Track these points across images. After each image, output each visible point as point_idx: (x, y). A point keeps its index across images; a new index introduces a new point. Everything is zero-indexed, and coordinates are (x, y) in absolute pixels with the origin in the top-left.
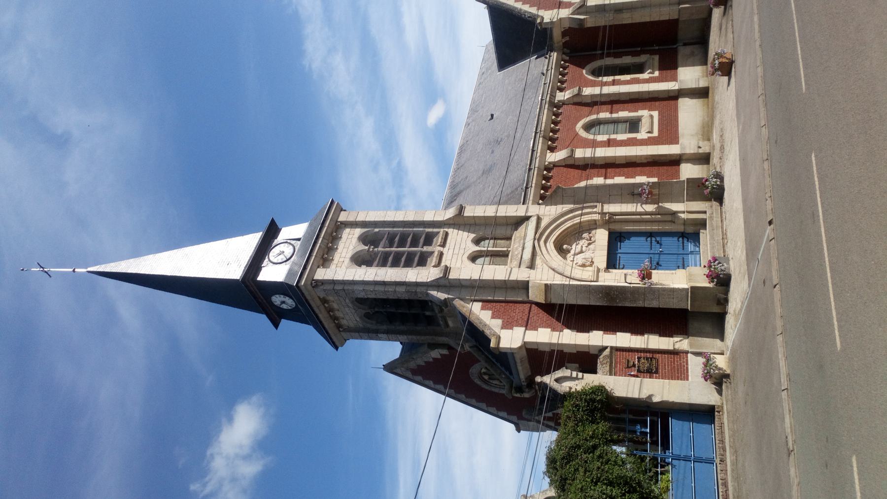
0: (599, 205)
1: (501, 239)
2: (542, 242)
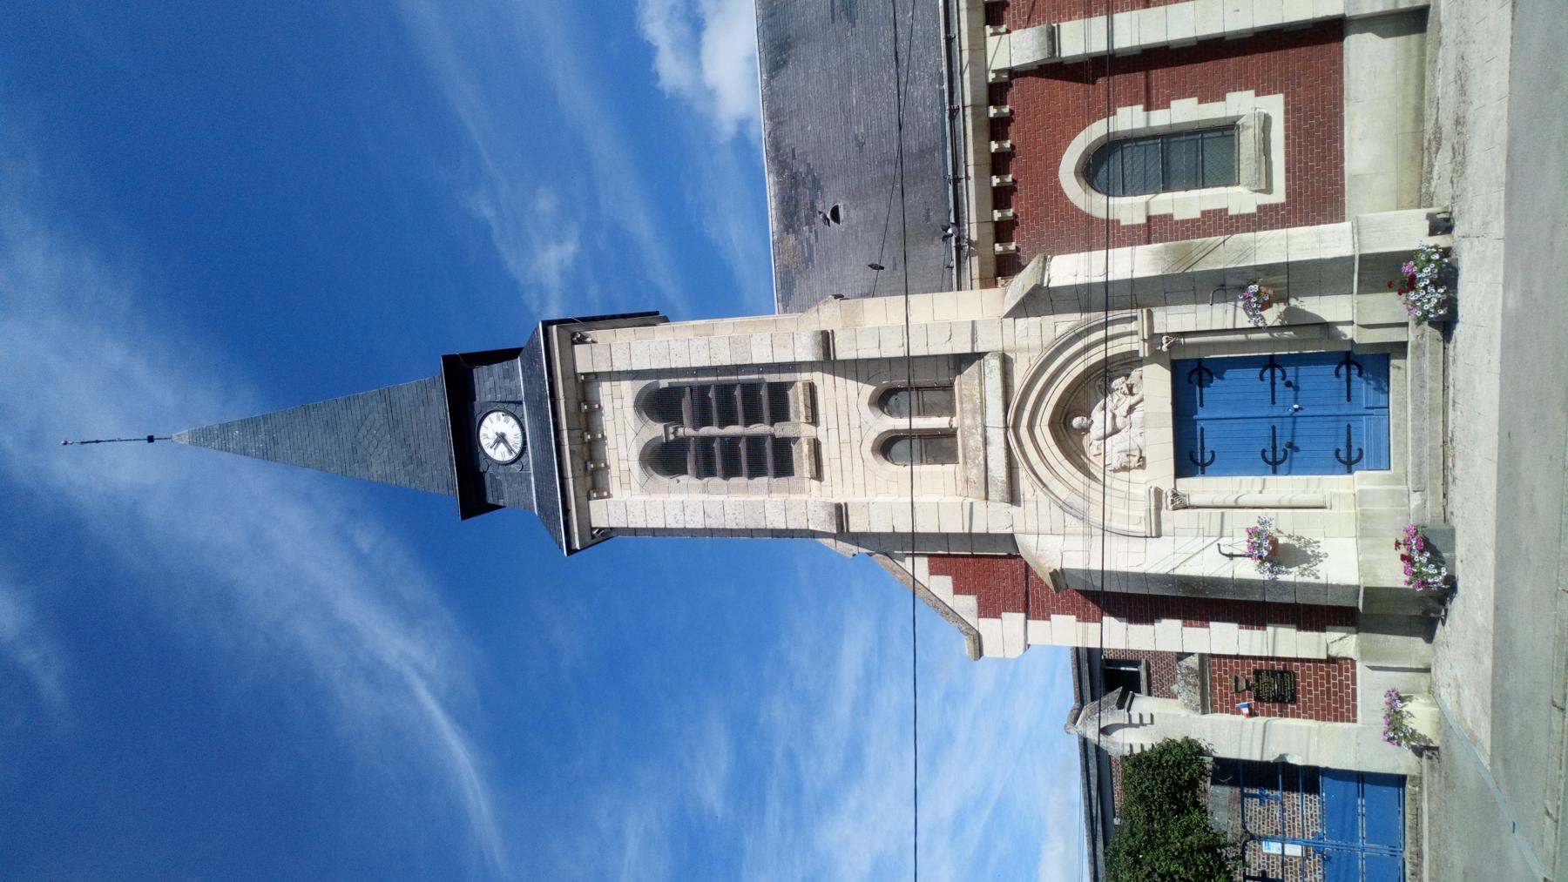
0: (1141, 313)
1: (932, 388)
2: (1023, 431)
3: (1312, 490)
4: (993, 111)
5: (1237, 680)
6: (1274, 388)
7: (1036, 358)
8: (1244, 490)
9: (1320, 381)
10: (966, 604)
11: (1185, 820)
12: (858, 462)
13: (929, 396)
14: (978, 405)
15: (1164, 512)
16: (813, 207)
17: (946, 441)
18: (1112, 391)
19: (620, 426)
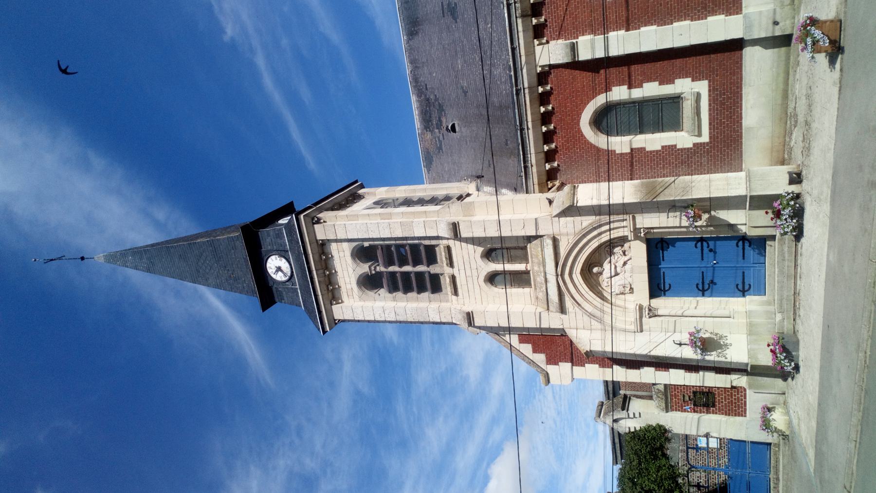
3: (723, 306)
4: (541, 90)
5: (684, 396)
6: (701, 257)
7: (572, 240)
8: (687, 306)
9: (727, 249)
10: (540, 358)
11: (657, 463)
12: (477, 287)
13: (513, 252)
14: (541, 261)
15: (644, 319)
16: (440, 121)
17: (525, 276)
18: (614, 254)
19: (344, 266)
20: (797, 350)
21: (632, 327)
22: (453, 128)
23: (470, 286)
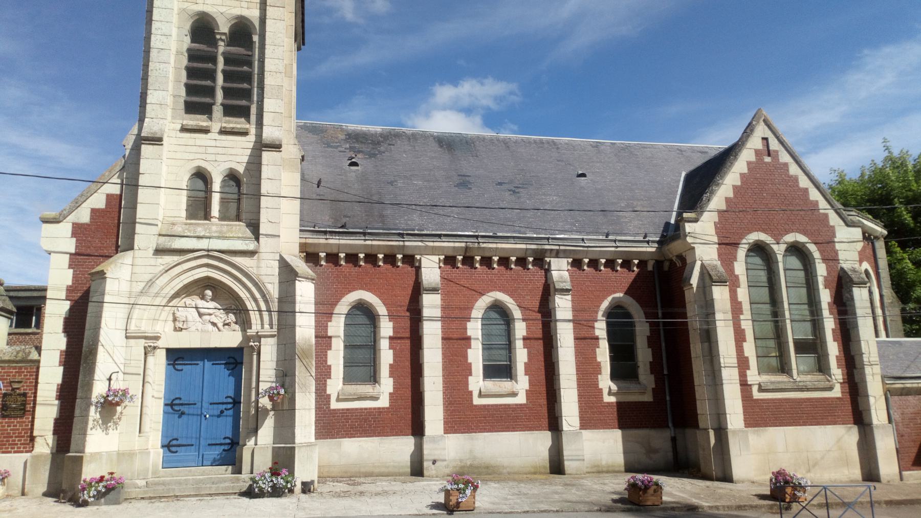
0: (274, 331)
2: (205, 261)
4: (400, 256)
6: (218, 402)
7: (253, 271)
8: (156, 387)
9: (224, 428)
10: (83, 216)
12: (192, 156)
15: (143, 341)
17: (202, 214)
18: (227, 313)
20: (106, 504)
21: (132, 328)
22: (354, 164)
23: (194, 149)
